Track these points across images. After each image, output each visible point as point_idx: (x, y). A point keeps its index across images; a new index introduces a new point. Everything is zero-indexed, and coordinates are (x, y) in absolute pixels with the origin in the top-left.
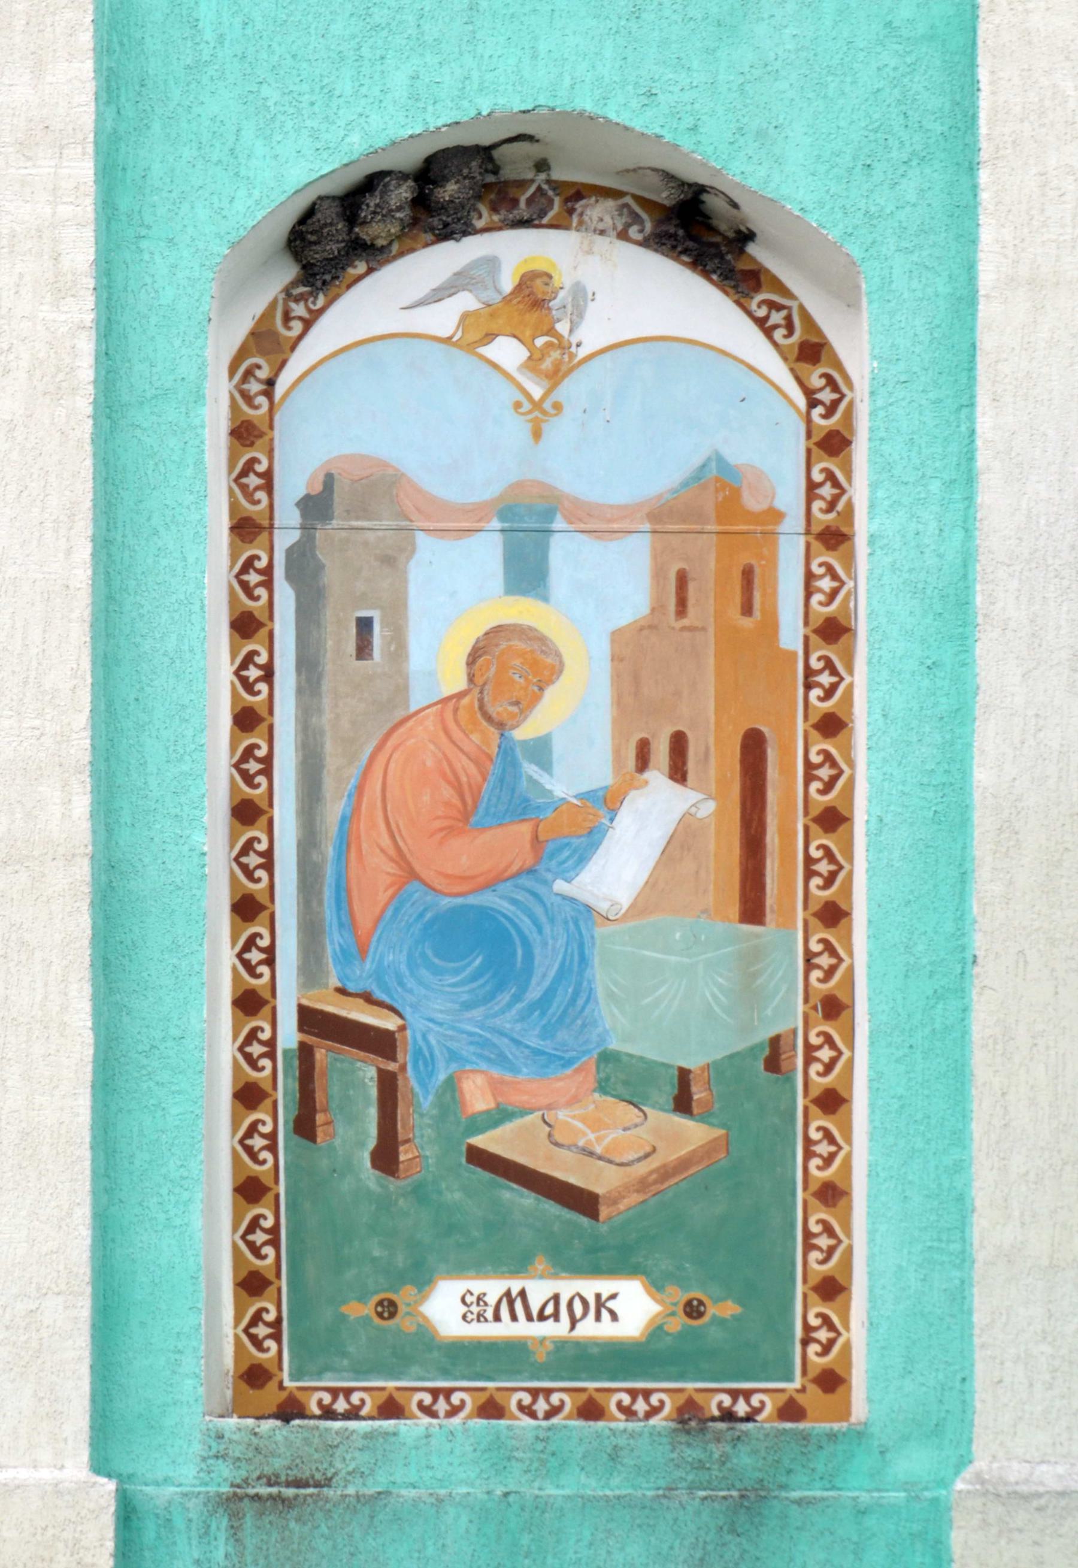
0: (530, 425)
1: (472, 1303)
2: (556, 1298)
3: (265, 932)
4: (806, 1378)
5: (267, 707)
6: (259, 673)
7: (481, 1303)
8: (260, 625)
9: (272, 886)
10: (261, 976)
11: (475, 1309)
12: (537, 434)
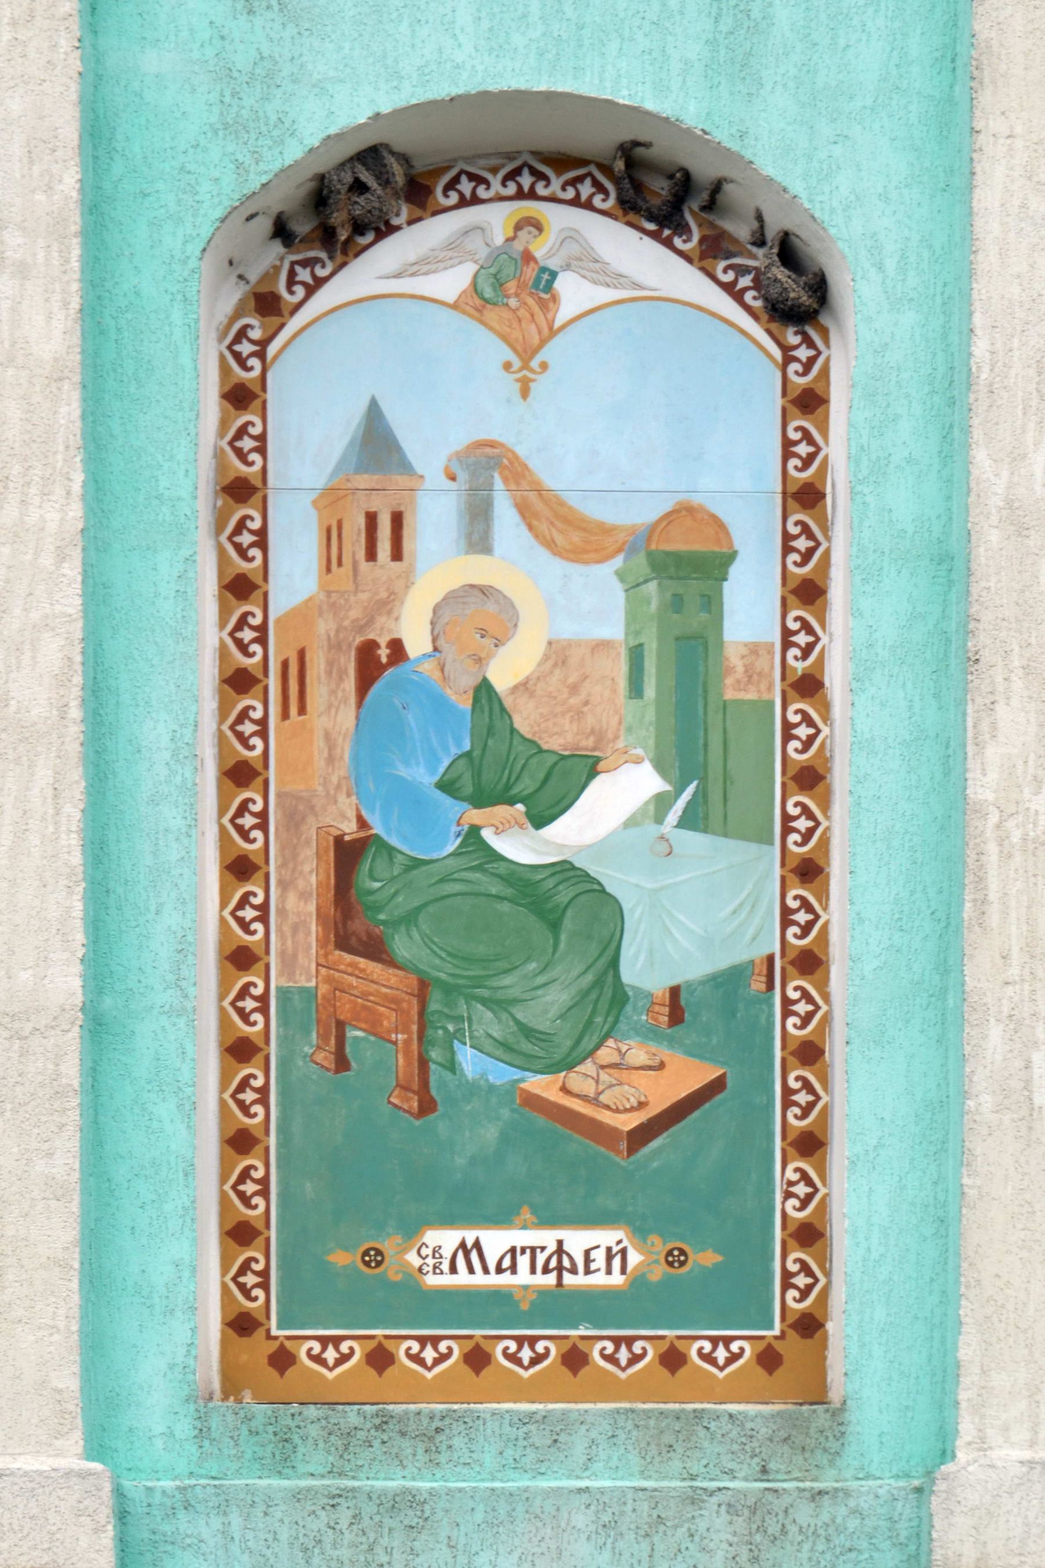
0: (518, 385)
1: (427, 1256)
3: (257, 515)
4: (266, 1327)
5: (263, 946)
6: (254, 821)
7: (437, 1255)
9: (264, 470)
10: (256, 1299)
11: (430, 1261)
12: (525, 393)
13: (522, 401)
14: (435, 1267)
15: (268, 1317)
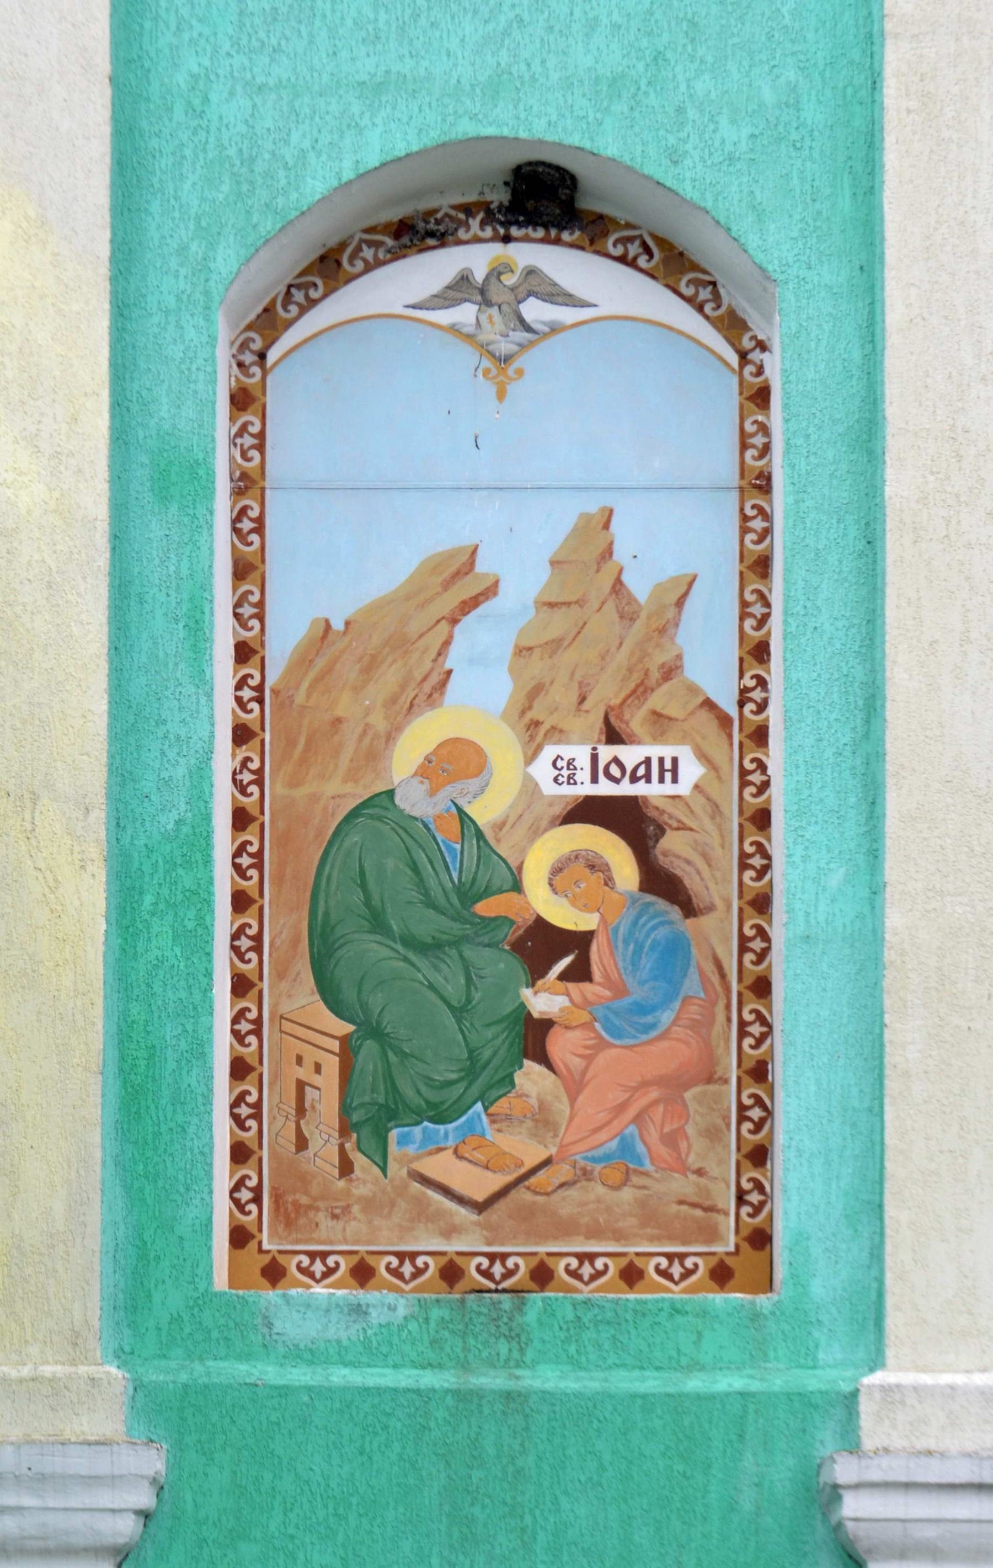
1: (562, 768)
2: (648, 761)
7: (571, 767)
8: (255, 652)
13: (497, 402)
14: (569, 778)
15: (260, 1230)
